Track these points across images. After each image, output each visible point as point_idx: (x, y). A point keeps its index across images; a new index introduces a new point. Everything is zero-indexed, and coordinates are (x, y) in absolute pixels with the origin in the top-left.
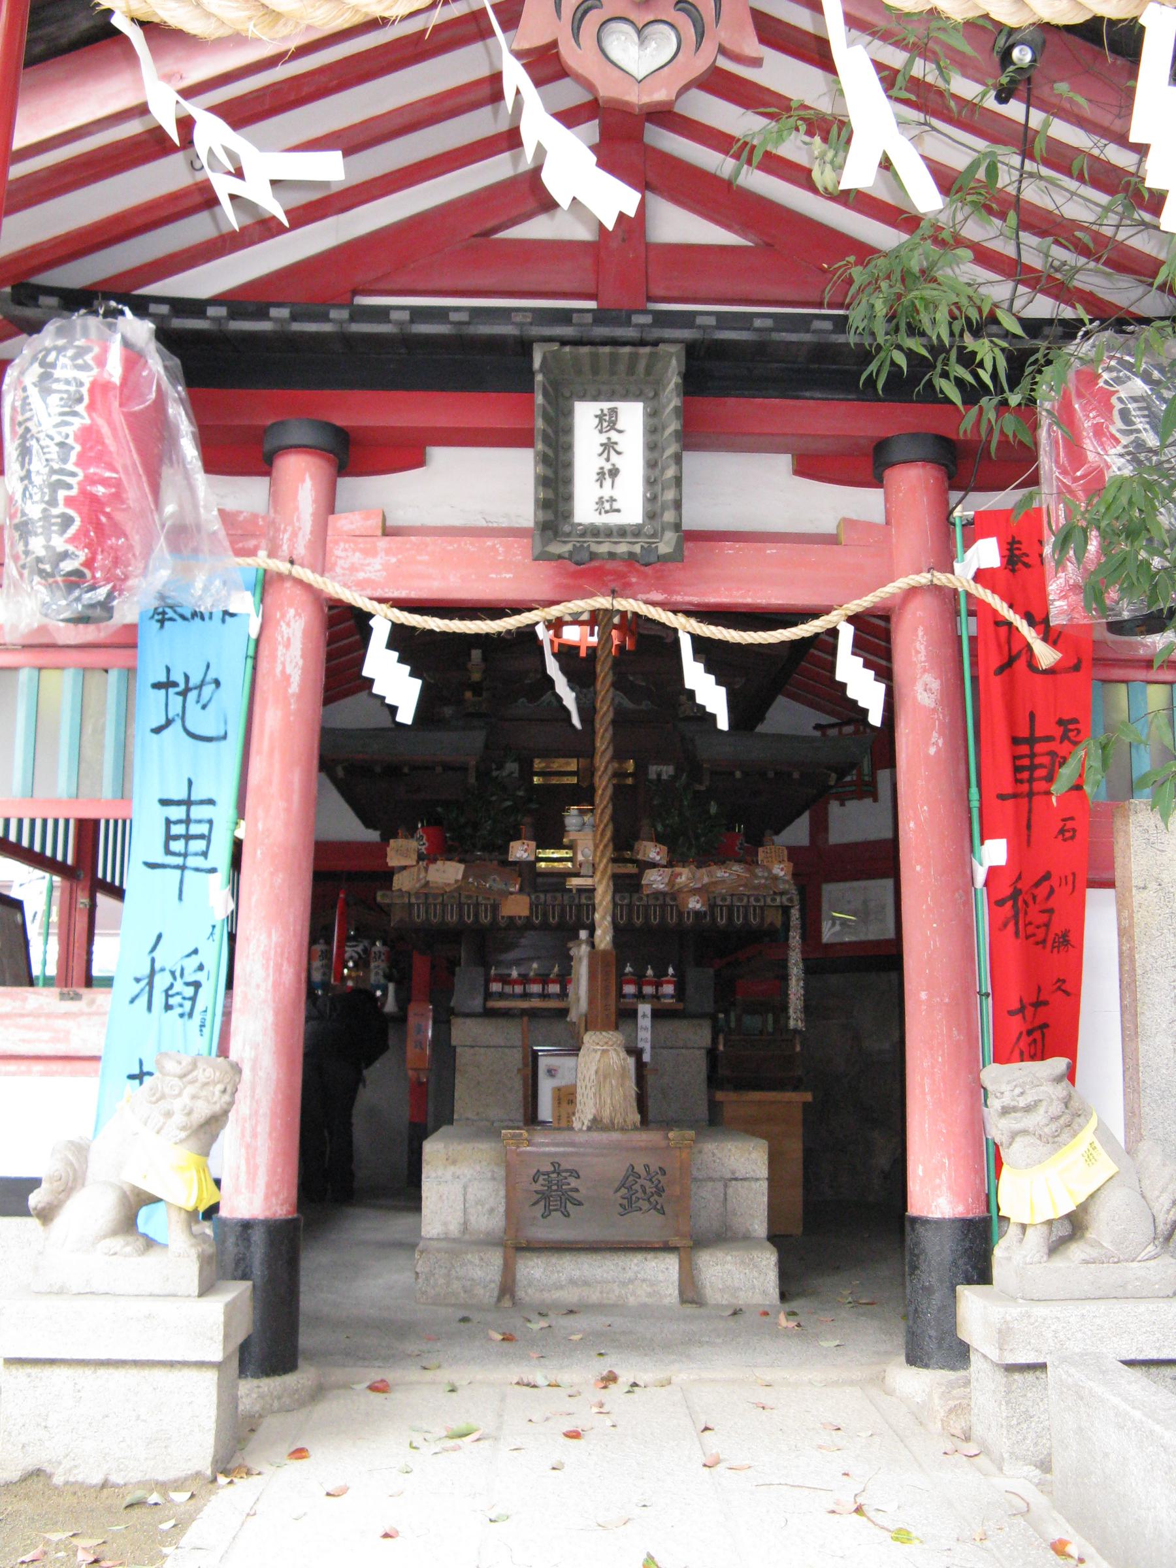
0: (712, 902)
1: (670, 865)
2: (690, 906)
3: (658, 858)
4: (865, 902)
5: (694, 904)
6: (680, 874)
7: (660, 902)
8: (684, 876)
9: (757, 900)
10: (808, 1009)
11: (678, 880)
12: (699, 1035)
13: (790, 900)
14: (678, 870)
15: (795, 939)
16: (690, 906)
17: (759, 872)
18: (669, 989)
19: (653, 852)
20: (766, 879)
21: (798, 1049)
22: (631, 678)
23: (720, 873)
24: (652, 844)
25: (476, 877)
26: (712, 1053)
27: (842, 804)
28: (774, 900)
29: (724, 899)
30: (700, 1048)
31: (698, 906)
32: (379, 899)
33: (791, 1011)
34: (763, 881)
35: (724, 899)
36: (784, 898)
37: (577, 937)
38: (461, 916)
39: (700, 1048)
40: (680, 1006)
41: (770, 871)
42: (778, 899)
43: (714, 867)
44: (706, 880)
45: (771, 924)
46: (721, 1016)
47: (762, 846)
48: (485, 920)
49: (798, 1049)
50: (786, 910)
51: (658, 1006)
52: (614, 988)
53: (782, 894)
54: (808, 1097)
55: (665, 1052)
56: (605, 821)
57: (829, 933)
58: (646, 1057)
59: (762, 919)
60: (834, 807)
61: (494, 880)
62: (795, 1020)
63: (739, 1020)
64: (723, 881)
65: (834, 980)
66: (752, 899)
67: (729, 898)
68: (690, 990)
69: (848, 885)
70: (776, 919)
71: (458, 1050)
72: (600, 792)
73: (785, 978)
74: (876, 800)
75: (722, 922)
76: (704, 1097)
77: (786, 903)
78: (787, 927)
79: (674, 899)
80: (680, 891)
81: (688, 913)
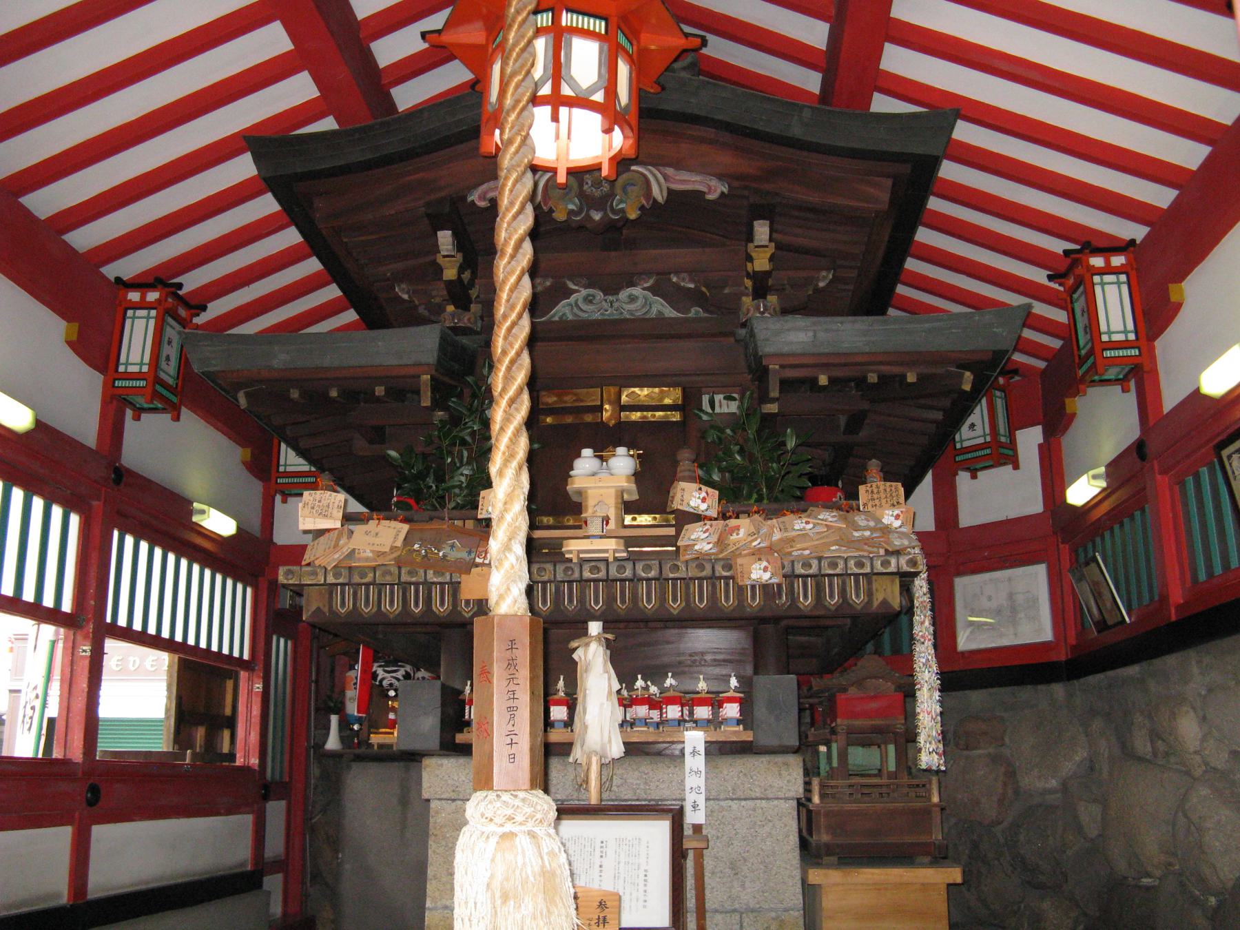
0: (788, 570)
1: (724, 516)
2: (754, 576)
3: (703, 507)
4: (1011, 596)
5: (759, 573)
6: (738, 528)
7: (707, 572)
8: (744, 529)
9: (860, 564)
10: (950, 738)
11: (734, 537)
12: (783, 779)
13: (913, 562)
14: (733, 522)
15: (923, 625)
16: (754, 576)
17: (860, 520)
18: (732, 710)
19: (694, 497)
20: (872, 530)
21: (935, 799)
22: (675, 279)
23: (799, 524)
24: (695, 486)
25: (423, 542)
26: (802, 804)
27: (974, 477)
28: (886, 563)
29: (807, 565)
30: (786, 799)
31: (766, 576)
32: (282, 579)
33: (922, 739)
34: (867, 533)
35: (807, 565)
36: (903, 560)
37: (584, 632)
38: (405, 602)
39: (786, 799)
40: (748, 736)
41: (879, 521)
42: (893, 561)
43: (790, 517)
44: (777, 536)
45: (885, 602)
46: (823, 749)
47: (864, 483)
48: (441, 608)
49: (935, 799)
50: (906, 580)
51: (720, 737)
52: (263, 636)
53: (897, 553)
54: (956, 875)
55: (734, 805)
56: (517, 346)
57: (965, 642)
58: (694, 817)
59: (870, 594)
60: (963, 478)
61: (452, 546)
62: (929, 755)
63: (843, 756)
64: (804, 536)
65: (977, 698)
66: (852, 563)
67: (815, 563)
68: (760, 711)
69: (987, 576)
70: (889, 594)
71: (433, 805)
72: (504, 296)
73: (909, 692)
74: (1016, 467)
75: (806, 602)
76: (797, 874)
77: (906, 568)
78: (910, 611)
79: (728, 567)
80: (736, 554)
81: (753, 587)
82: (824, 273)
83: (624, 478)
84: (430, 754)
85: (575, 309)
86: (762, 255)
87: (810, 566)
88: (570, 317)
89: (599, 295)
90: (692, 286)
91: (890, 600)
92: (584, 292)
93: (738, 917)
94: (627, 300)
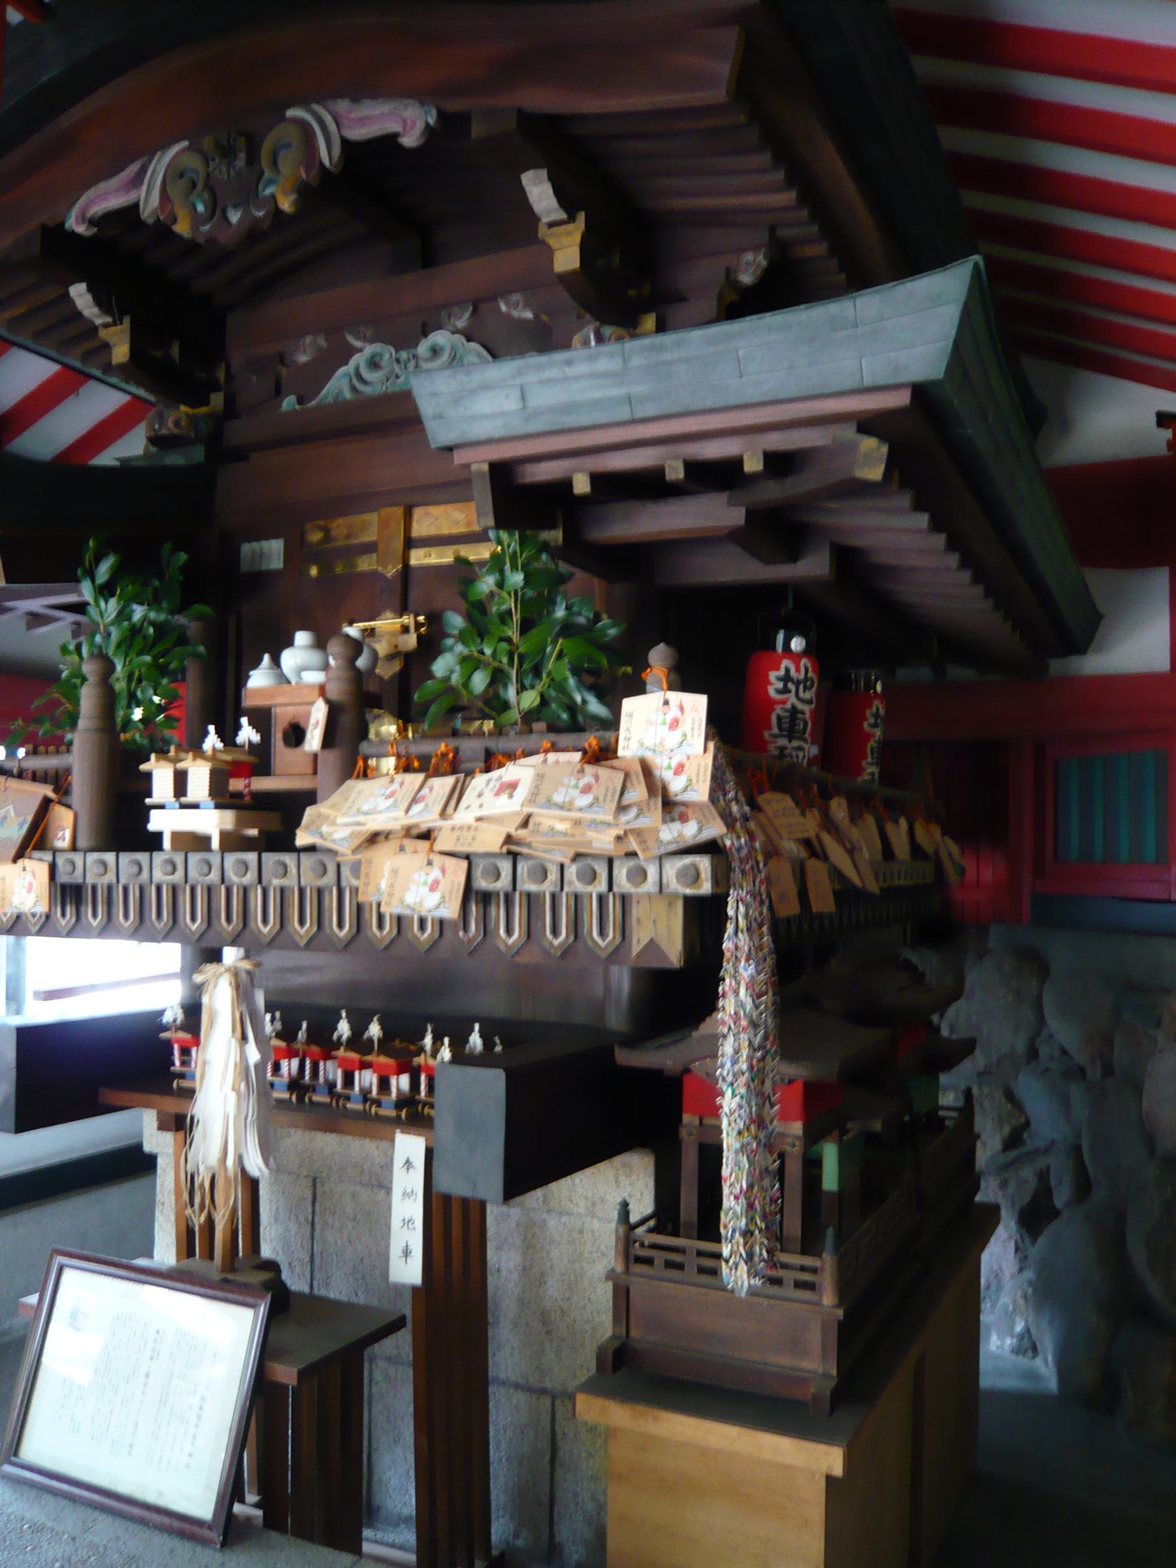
2: (410, 898)
82: (749, 257)
83: (1164, 444)
84: (619, 857)
85: (355, 381)
86: (565, 241)
87: (498, 876)
88: (348, 395)
89: (387, 352)
90: (528, 315)
91: (664, 946)
92: (369, 350)
93: (548, 1402)
94: (428, 354)
